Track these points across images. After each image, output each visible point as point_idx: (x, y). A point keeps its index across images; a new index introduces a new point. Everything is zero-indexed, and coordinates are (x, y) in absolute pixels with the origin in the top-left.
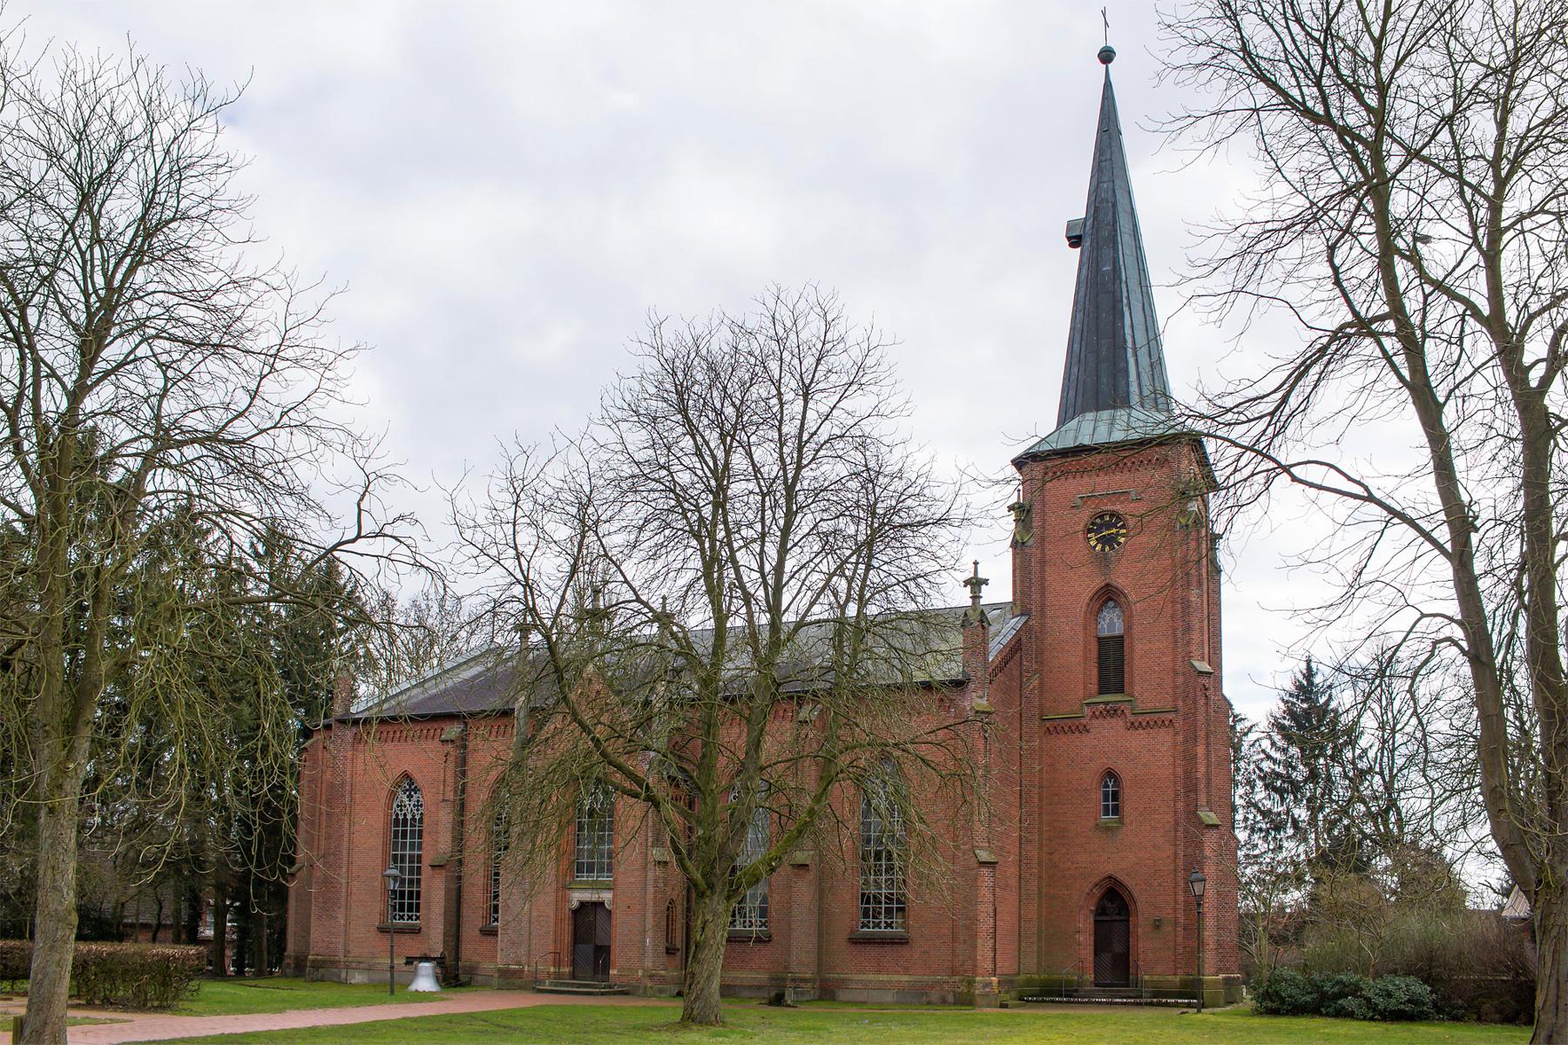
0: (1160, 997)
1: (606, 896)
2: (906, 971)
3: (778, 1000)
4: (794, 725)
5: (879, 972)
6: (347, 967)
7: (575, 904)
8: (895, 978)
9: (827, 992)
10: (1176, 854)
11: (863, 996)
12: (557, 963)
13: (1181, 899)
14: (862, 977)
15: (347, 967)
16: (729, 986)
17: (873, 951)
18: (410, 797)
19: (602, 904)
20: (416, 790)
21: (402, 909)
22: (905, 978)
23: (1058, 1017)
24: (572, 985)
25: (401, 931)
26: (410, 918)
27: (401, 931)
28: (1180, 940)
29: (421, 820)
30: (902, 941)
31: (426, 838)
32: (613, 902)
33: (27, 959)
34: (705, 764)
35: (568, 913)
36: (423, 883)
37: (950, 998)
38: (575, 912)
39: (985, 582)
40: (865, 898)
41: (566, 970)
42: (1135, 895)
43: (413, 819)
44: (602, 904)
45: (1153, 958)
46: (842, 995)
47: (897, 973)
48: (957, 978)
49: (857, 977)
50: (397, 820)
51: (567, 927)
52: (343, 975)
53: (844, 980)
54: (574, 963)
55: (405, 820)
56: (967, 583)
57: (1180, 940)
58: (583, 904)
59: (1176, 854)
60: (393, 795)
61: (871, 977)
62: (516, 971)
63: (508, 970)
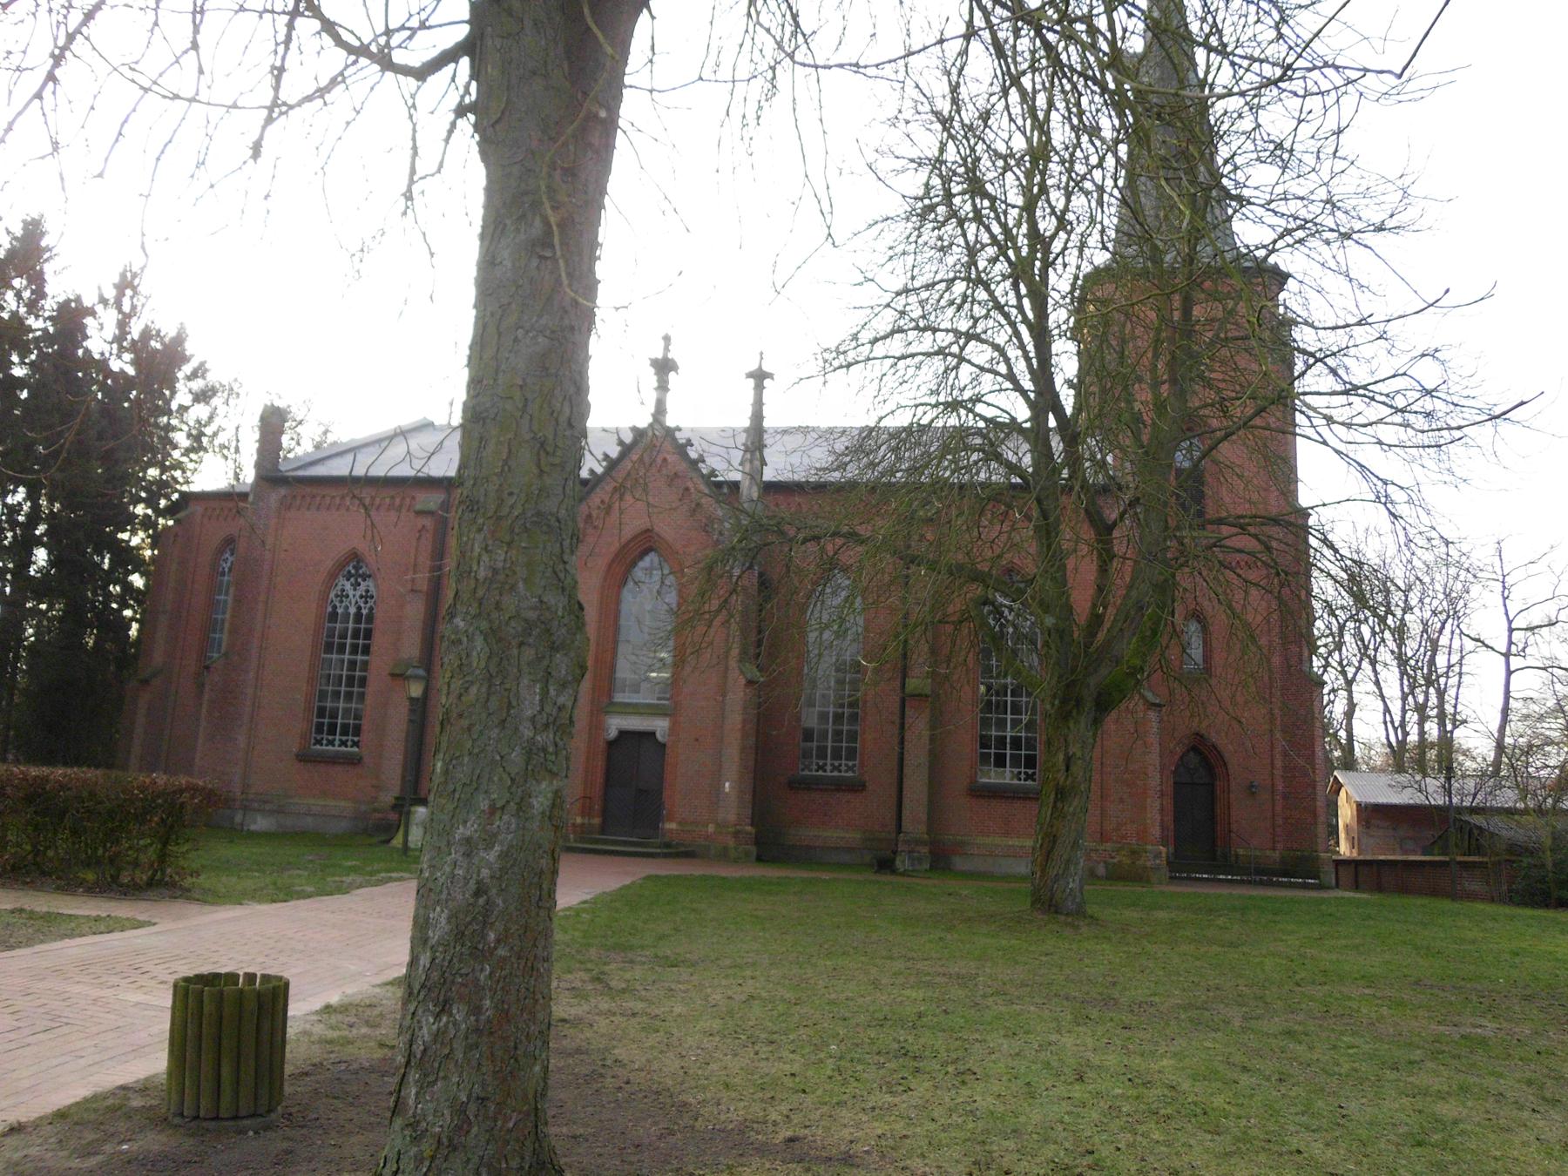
0: (1262, 874)
1: (660, 726)
3: (885, 865)
4: (412, 515)
5: (1007, 834)
6: (245, 809)
7: (613, 734)
9: (940, 859)
10: (1271, 712)
12: (585, 812)
13: (1279, 763)
14: (988, 840)
15: (245, 809)
16: (758, 841)
19: (653, 734)
20: (365, 577)
23: (1532, 917)
25: (333, 760)
26: (343, 743)
27: (333, 760)
28: (1278, 809)
29: (370, 618)
31: (378, 641)
32: (673, 730)
34: (1361, 590)
35: (602, 744)
36: (369, 699)
37: (1101, 870)
38: (611, 744)
39: (770, 376)
41: (596, 821)
42: (1226, 756)
44: (653, 734)
45: (1250, 825)
46: (959, 863)
48: (1109, 846)
49: (979, 840)
50: (333, 616)
51: (600, 763)
52: (238, 818)
54: (605, 813)
56: (750, 375)
57: (1278, 809)
58: (623, 734)
59: (1271, 712)
60: (333, 576)
61: (997, 840)
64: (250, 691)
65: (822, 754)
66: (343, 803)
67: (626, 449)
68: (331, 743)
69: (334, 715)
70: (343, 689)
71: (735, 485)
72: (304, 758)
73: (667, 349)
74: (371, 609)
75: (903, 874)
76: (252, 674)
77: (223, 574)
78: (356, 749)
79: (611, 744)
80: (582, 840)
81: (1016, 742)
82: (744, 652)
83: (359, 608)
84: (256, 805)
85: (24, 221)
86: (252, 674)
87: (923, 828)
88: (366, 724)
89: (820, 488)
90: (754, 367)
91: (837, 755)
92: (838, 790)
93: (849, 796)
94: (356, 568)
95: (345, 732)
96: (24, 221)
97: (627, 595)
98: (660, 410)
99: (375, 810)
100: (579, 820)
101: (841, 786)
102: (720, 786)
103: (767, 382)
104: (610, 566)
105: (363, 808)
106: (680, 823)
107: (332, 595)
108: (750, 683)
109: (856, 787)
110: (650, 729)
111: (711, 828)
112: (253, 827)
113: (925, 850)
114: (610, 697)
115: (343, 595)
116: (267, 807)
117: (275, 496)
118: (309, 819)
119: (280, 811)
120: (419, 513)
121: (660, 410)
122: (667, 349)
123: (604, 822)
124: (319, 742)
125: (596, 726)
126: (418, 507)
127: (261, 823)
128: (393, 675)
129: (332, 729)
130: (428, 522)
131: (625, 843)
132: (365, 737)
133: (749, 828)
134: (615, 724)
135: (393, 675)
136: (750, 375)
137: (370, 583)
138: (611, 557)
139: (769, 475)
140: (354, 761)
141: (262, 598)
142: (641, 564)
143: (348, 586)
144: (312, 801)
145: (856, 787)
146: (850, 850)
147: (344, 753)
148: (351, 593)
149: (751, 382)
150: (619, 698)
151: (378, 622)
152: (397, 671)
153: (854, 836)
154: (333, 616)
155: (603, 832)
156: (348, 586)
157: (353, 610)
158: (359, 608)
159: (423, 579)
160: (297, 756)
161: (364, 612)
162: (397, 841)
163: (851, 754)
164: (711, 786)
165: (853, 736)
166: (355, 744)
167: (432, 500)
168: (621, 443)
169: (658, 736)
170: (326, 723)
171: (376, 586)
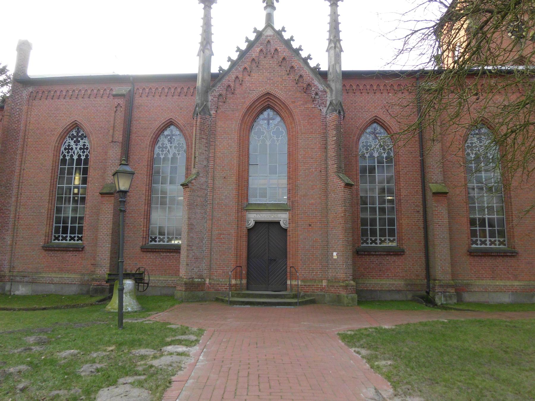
1: (283, 218)
2: (516, 278)
5: (493, 278)
6: (12, 281)
7: (252, 224)
8: (508, 283)
11: (483, 298)
14: (484, 282)
17: (488, 262)
18: (77, 142)
20: (83, 137)
21: (65, 230)
22: (516, 283)
24: (248, 296)
25: (66, 249)
26: (72, 239)
27: (66, 249)
29: (86, 161)
30: (511, 254)
32: (292, 220)
33: (479, 219)
35: (245, 232)
40: (473, 222)
41: (244, 281)
43: (79, 161)
44: (278, 223)
46: (467, 297)
47: (509, 279)
49: (478, 282)
50: (64, 161)
51: (244, 244)
52: (7, 288)
53: (468, 285)
55: (72, 159)
58: (258, 223)
61: (489, 282)
62: (199, 284)
63: (346, 335)
64: (12, 209)
65: (373, 233)
66: (73, 276)
67: (251, 45)
68: (65, 238)
69: (65, 221)
70: (64, 196)
72: (48, 248)
74: (87, 156)
75: (444, 307)
76: (14, 199)
78: (80, 242)
79: (249, 230)
80: (239, 295)
82: (339, 168)
83: (80, 156)
84: (18, 279)
86: (14, 199)
87: (449, 277)
88: (86, 225)
91: (383, 233)
92: (387, 255)
93: (395, 258)
94: (78, 133)
95: (73, 231)
97: (253, 137)
98: (269, 18)
99: (93, 279)
100: (233, 282)
102: (327, 255)
104: (244, 117)
105: (86, 278)
106: (303, 280)
107: (62, 149)
109: (398, 253)
110: (276, 219)
111: (324, 283)
112: (17, 293)
113: (452, 291)
114: (247, 200)
115: (69, 148)
116: (26, 279)
117: (25, 93)
118: (52, 286)
119: (33, 282)
120: (115, 96)
121: (269, 18)
123: (248, 283)
124: (57, 238)
125: (241, 219)
126: (114, 93)
127: (21, 290)
128: (101, 194)
129: (65, 232)
130: (121, 101)
131: (261, 296)
132: (86, 234)
133: (352, 282)
134: (252, 218)
135: (101, 194)
137: (86, 140)
138: (244, 110)
140: (79, 249)
141: (19, 152)
142: (261, 117)
143: (72, 143)
144: (53, 275)
145: (398, 253)
146: (399, 291)
147: (73, 244)
148: (74, 147)
150: (252, 201)
151: (91, 163)
152: (104, 191)
153: (399, 283)
154: (64, 161)
155: (248, 289)
156: (72, 143)
157: (75, 157)
158: (80, 156)
159: (119, 137)
160: (43, 247)
161: (83, 158)
162: (113, 305)
163: (392, 233)
164: (323, 253)
165: (391, 222)
166: (80, 239)
169: (281, 223)
170: (62, 227)
171: (90, 142)
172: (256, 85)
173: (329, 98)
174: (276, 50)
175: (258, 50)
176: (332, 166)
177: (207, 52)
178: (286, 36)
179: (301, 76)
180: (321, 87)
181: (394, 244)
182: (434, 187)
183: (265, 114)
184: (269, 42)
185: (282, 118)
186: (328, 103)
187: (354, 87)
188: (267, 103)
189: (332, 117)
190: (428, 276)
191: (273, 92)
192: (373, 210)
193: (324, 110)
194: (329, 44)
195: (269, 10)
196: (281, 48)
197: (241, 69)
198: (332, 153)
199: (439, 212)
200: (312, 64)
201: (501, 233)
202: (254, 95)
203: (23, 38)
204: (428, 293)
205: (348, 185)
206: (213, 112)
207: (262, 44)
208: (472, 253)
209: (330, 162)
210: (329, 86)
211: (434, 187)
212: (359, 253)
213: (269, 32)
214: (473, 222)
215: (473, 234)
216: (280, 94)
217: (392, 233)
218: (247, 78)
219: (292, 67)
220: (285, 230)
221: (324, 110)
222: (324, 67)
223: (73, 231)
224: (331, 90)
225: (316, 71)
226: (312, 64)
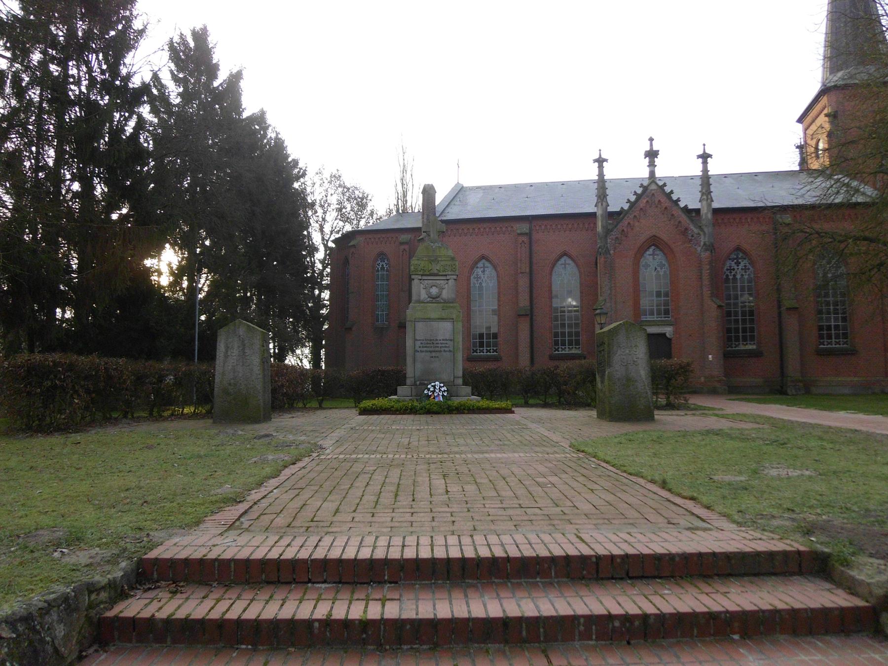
1: (668, 331)
8: (849, 379)
14: (829, 379)
19: (664, 334)
22: (856, 379)
26: (488, 351)
30: (852, 352)
39: (606, 160)
40: (821, 328)
56: (699, 157)
67: (639, 197)
71: (698, 211)
73: (651, 145)
77: (378, 271)
81: (837, 327)
83: (742, 275)
85: (263, 113)
89: (813, 207)
90: (701, 152)
95: (488, 345)
96: (263, 113)
101: (750, 354)
103: (605, 164)
108: (720, 307)
111: (702, 379)
122: (651, 145)
136: (699, 157)
139: (715, 205)
148: (736, 267)
149: (597, 164)
161: (731, 277)
165: (752, 330)
166: (495, 351)
167: (524, 227)
168: (635, 193)
169: (668, 335)
172: (645, 228)
173: (703, 240)
174: (659, 201)
175: (645, 201)
176: (707, 292)
177: (604, 204)
178: (667, 189)
179: (680, 222)
180: (696, 231)
181: (754, 347)
182: (787, 304)
183: (562, 260)
184: (653, 194)
185: (665, 254)
186: (702, 243)
187: (720, 221)
188: (655, 242)
189: (705, 255)
190: (783, 374)
191: (657, 235)
192: (737, 321)
193: (699, 249)
194: (702, 195)
195: (652, 168)
196: (663, 199)
197: (632, 216)
198: (706, 282)
199: (792, 323)
200: (682, 204)
201: (845, 336)
202: (643, 238)
203: (429, 182)
204: (782, 387)
205: (720, 307)
206: (612, 252)
207: (648, 196)
208: (820, 353)
209: (705, 289)
210: (702, 230)
211: (787, 304)
212: (728, 356)
213: (653, 187)
214: (821, 328)
215: (821, 337)
216: (664, 237)
217: (752, 338)
218: (637, 224)
219: (673, 215)
220: (670, 339)
221: (699, 249)
222: (694, 204)
223: (488, 345)
224: (705, 234)
225: (686, 210)
226: (682, 204)
